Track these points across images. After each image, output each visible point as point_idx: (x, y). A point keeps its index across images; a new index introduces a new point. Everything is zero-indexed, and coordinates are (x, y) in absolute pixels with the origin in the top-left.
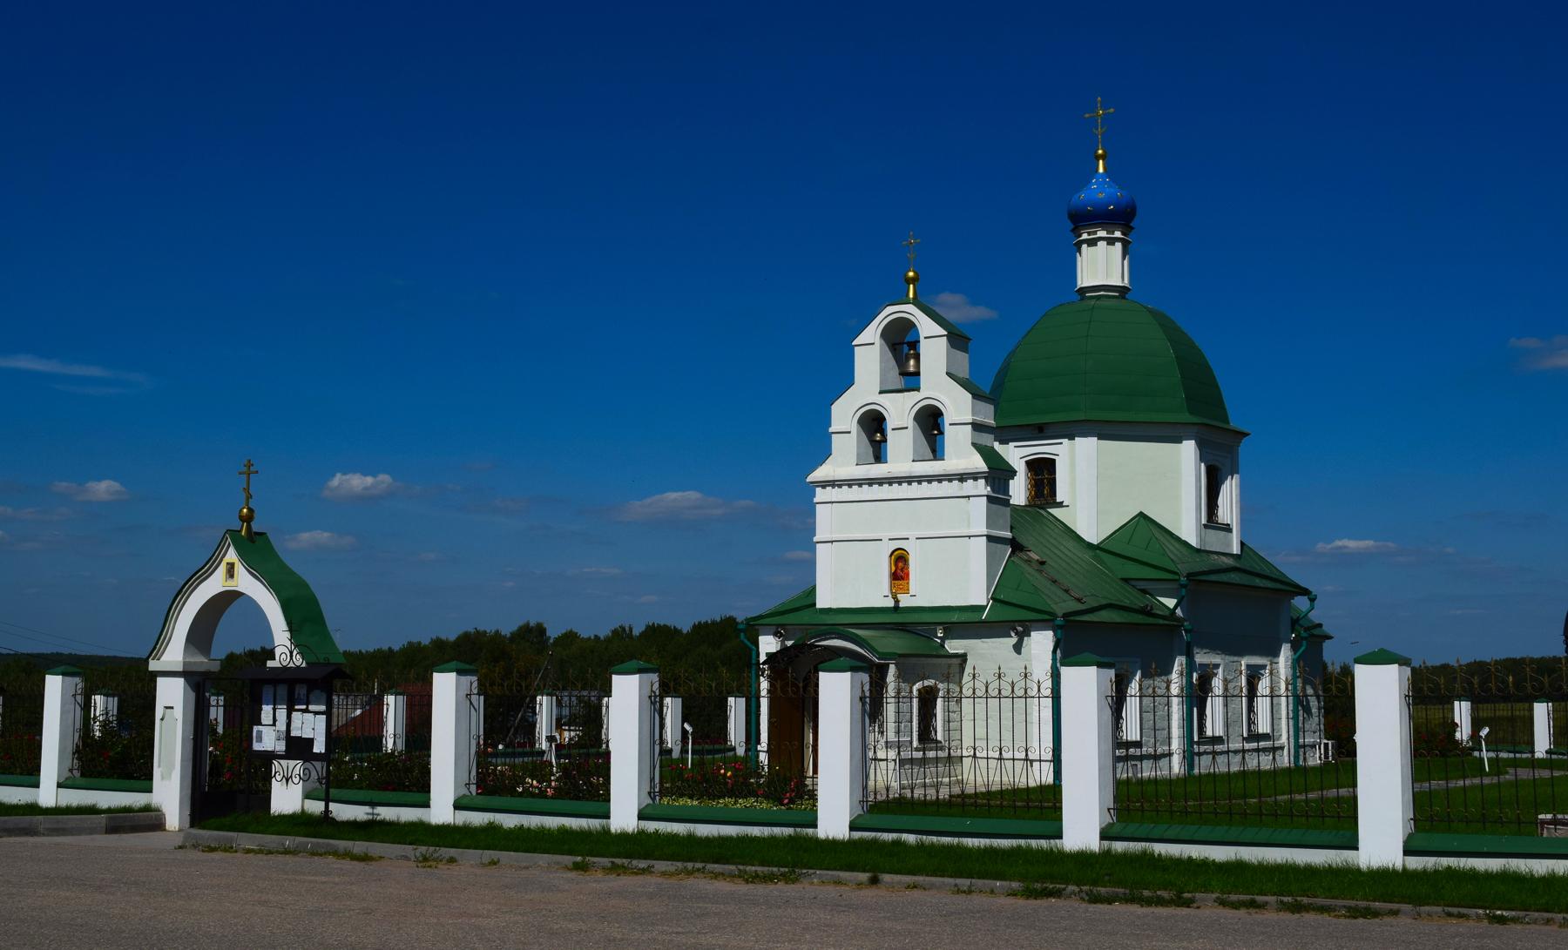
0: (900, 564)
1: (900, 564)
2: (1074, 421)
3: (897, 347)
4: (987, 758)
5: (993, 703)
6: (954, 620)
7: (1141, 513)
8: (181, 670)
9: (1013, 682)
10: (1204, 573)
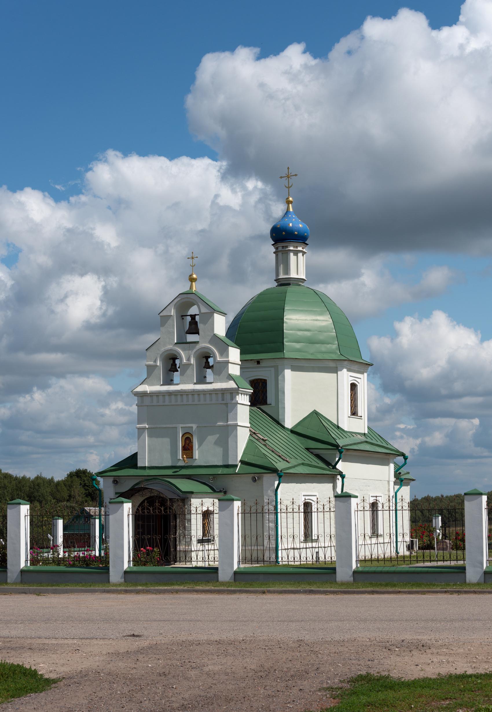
0: (187, 442)
1: (187, 442)
2: (150, 347)
3: (183, 317)
4: (384, 543)
5: (327, 515)
6: (220, 473)
7: (315, 410)
8: (235, 502)
9: (196, 507)
10: (351, 445)
